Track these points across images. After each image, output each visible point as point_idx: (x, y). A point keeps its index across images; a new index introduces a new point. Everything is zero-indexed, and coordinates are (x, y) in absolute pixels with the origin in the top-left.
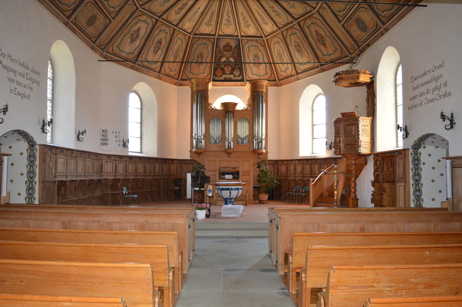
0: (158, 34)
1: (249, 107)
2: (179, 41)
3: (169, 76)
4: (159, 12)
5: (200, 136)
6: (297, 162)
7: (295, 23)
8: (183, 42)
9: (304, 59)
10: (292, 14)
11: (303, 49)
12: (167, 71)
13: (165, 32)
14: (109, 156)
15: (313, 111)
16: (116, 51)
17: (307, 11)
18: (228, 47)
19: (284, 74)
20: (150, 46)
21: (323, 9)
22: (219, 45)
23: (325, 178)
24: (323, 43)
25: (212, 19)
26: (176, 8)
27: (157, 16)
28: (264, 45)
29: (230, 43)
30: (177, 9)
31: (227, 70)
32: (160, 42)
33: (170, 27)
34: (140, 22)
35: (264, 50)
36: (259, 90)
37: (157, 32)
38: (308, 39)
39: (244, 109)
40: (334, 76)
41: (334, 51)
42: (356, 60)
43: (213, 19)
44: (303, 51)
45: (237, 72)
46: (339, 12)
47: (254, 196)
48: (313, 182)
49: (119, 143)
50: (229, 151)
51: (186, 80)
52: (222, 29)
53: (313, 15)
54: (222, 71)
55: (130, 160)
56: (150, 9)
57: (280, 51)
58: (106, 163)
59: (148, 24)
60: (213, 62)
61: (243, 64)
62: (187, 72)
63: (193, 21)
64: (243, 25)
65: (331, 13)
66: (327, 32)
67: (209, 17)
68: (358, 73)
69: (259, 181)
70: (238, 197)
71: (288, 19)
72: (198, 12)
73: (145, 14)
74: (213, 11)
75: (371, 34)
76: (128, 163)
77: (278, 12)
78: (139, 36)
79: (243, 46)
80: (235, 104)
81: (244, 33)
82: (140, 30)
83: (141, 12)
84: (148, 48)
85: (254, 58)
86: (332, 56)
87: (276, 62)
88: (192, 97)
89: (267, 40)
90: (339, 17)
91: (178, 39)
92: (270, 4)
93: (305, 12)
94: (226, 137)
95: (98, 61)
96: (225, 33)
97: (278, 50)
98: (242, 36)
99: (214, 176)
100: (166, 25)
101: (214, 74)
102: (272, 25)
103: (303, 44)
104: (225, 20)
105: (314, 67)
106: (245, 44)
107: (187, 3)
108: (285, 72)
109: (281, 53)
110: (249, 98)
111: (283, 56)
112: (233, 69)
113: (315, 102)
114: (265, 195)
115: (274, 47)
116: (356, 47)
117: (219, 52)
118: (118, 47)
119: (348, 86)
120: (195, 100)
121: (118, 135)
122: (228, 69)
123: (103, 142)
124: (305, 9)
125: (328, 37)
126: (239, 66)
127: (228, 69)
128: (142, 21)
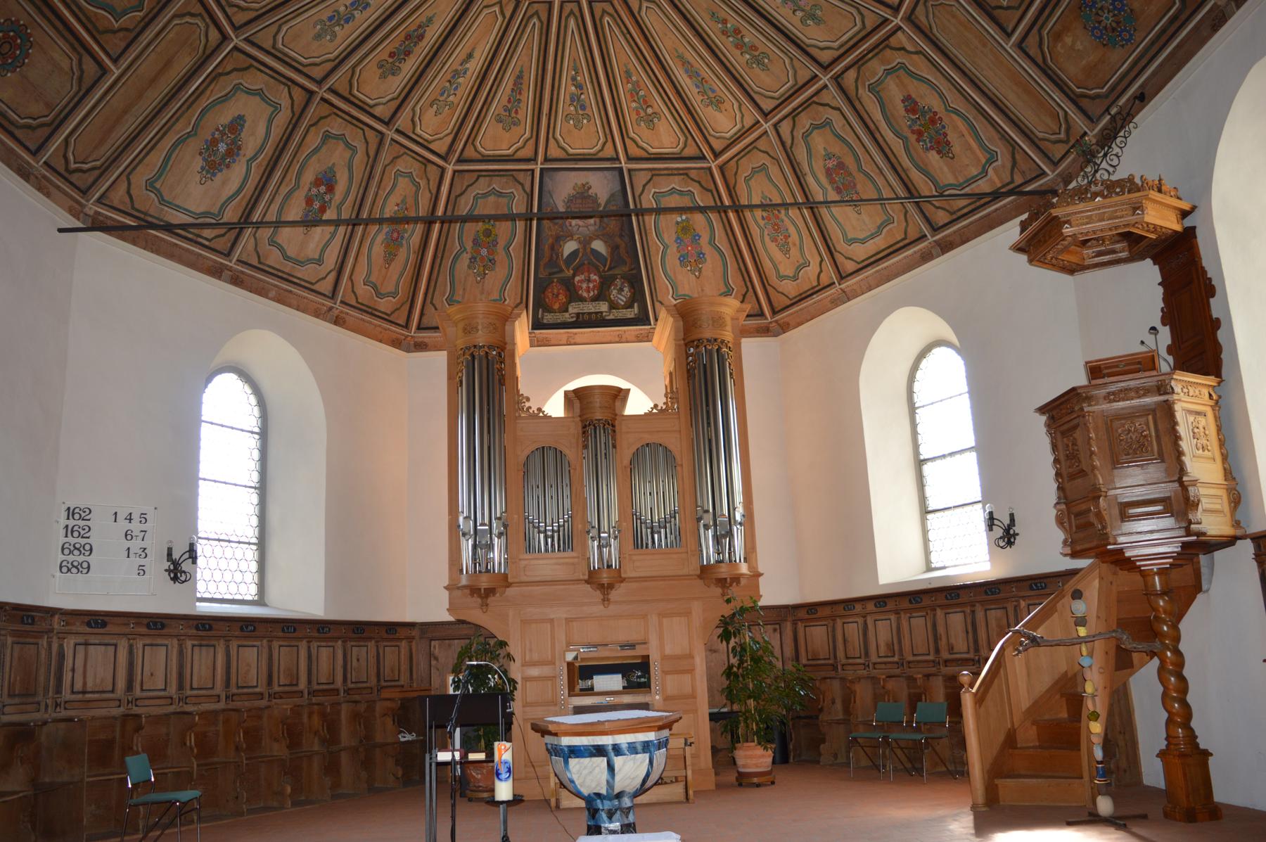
2: (403, 183)
5: (486, 521)
6: (870, 606)
8: (418, 186)
10: (808, 49)
11: (859, 178)
14: (97, 620)
15: (912, 409)
16: (148, 202)
18: (583, 207)
19: (790, 288)
20: (290, 193)
23: (1017, 664)
28: (712, 187)
31: (584, 286)
33: (365, 128)
34: (242, 97)
37: (314, 140)
38: (878, 136)
39: (655, 411)
41: (984, 167)
42: (1105, 155)
43: (523, 97)
45: (621, 290)
47: (715, 750)
48: (972, 686)
49: (142, 562)
50: (605, 578)
53: (891, 39)
54: (569, 290)
55: (201, 633)
58: (81, 649)
59: (276, 107)
63: (453, 107)
64: (634, 116)
66: (951, 96)
69: (730, 694)
70: (649, 783)
72: (465, 73)
76: (189, 643)
77: (756, 49)
78: (239, 148)
79: (637, 194)
80: (619, 395)
82: (243, 126)
85: (678, 238)
89: (721, 169)
91: (399, 174)
92: (725, 22)
94: (591, 523)
95: (61, 230)
96: (571, 151)
99: (550, 683)
101: (540, 304)
102: (736, 106)
103: (858, 160)
104: (568, 101)
106: (644, 186)
107: (421, 31)
108: (795, 278)
114: (760, 751)
115: (749, 187)
118: (150, 185)
120: (461, 385)
121: (135, 526)
122: (589, 281)
123: (71, 558)
125: (956, 112)
126: (626, 269)
127: (589, 281)
128: (250, 92)
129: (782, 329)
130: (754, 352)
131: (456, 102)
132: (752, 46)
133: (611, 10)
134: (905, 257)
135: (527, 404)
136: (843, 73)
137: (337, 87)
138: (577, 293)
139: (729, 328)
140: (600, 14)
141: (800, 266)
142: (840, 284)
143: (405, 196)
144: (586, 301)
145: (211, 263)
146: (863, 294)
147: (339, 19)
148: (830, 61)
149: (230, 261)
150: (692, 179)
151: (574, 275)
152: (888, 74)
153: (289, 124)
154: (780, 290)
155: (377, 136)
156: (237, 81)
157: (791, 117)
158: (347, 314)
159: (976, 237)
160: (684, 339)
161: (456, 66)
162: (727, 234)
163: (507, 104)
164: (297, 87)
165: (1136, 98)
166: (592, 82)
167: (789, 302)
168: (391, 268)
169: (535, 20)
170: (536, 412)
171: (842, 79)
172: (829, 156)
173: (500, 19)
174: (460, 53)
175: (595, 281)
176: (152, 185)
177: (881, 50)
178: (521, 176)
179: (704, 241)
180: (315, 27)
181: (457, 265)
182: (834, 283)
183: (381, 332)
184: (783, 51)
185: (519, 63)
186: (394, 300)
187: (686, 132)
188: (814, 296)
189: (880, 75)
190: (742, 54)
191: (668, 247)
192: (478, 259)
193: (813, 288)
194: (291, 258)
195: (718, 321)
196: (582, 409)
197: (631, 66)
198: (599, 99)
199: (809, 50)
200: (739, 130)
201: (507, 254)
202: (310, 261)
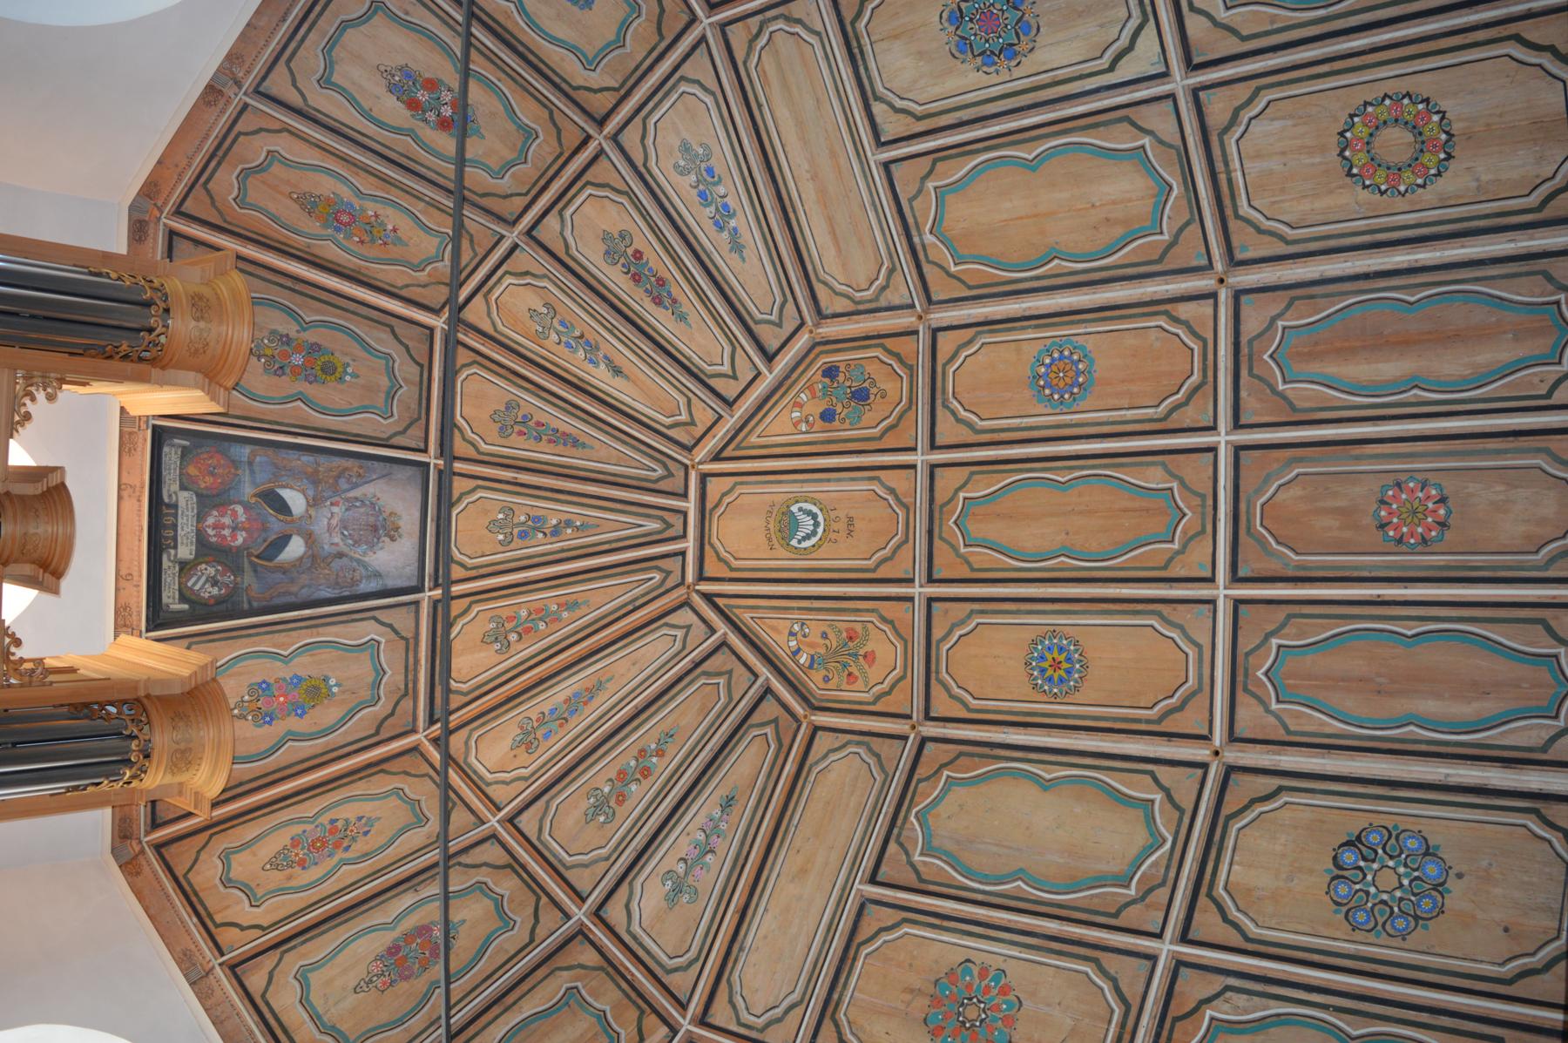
3: (219, 153)
4: (649, 141)
9: (352, 1000)
19: (207, 874)
28: (384, 735)
31: (227, 520)
33: (529, 198)
37: (528, 113)
38: (496, 1010)
39: (7, 640)
43: (544, 446)
45: (215, 583)
52: (480, 494)
53: (653, 1017)
56: (683, 87)
57: (361, 839)
63: (539, 338)
64: (505, 613)
67: (556, 424)
72: (591, 361)
77: (620, 803)
79: (377, 614)
85: (300, 679)
89: (415, 749)
92: (660, 753)
106: (390, 626)
107: (667, 302)
108: (227, 882)
110: (72, 670)
115: (386, 795)
122: (235, 529)
127: (235, 529)
128: (625, 26)
129: (127, 863)
130: (101, 820)
131: (546, 343)
132: (624, 796)
133: (670, 583)
137: (603, 161)
139: (169, 779)
140: (664, 567)
141: (251, 889)
142: (220, 965)
143: (407, 245)
144: (198, 522)
146: (206, 1010)
148: (608, 920)
152: (599, 1017)
153: (561, 77)
154: (203, 856)
155: (511, 214)
156: (644, 11)
157: (511, 861)
158: (223, 111)
160: (148, 696)
161: (605, 349)
162: (302, 761)
163: (535, 419)
164: (614, 102)
166: (563, 550)
167: (180, 872)
168: (289, 202)
169: (660, 472)
170: (23, 410)
171: (581, 943)
173: (668, 421)
174: (625, 357)
175: (234, 537)
177: (634, 1003)
178: (416, 431)
179: (294, 724)
181: (277, 314)
182: (222, 955)
183: (177, 166)
184: (619, 844)
185: (597, 444)
186: (230, 198)
187: (477, 693)
188: (195, 919)
189: (596, 1004)
190: (610, 780)
191: (286, 663)
192: (286, 348)
193: (210, 916)
194: (341, 35)
195: (184, 758)
196: (22, 499)
197: (584, 610)
198: (536, 560)
199: (625, 887)
200: (481, 778)
201: (292, 396)
202: (330, 65)
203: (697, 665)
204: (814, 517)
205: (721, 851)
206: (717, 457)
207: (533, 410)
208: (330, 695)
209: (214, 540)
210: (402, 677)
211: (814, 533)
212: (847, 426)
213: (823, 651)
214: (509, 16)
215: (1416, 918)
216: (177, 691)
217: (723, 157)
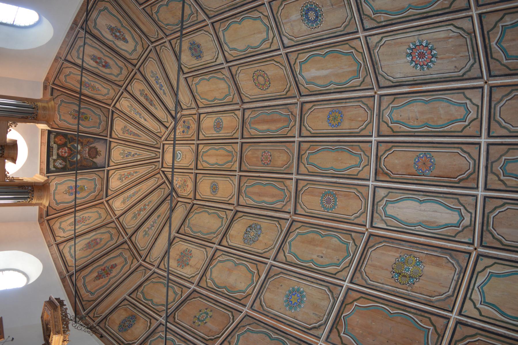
0: (117, 64)
1: (9, 180)
3: (59, 72)
7: (126, 238)
8: (104, 96)
10: (136, 233)
11: (92, 250)
12: (67, 71)
13: (118, 75)
17: (140, 252)
18: (94, 153)
19: (56, 227)
20: (102, 52)
21: (144, 271)
22: (98, 142)
24: (100, 276)
25: (131, 134)
26: (148, 91)
27: (140, 66)
29: (99, 156)
30: (146, 92)
31: (63, 151)
32: (106, 66)
33: (124, 81)
34: (134, 44)
35: (89, 200)
36: (35, 194)
37: (120, 64)
39: (6, 173)
40: (58, 297)
41: (90, 291)
42: (81, 325)
43: (132, 136)
44: (89, 250)
45: (61, 164)
46: (142, 293)
51: (52, 95)
54: (62, 145)
56: (150, 59)
59: (131, 54)
60: (80, 134)
61: (75, 172)
62: (63, 97)
63: (130, 112)
64: (122, 173)
65: (140, 283)
67: (134, 131)
68: (64, 332)
71: (130, 228)
72: (140, 117)
73: (143, 52)
74: (141, 137)
75: (118, 338)
77: (139, 215)
78: (117, 39)
79: (96, 173)
81: (112, 174)
82: (125, 42)
83: (147, 46)
84: (100, 48)
86: (84, 289)
87: (77, 214)
88: (27, 99)
89: (102, 203)
90: (135, 293)
91: (109, 90)
92: (148, 205)
93: (139, 249)
96: (113, 150)
97: (90, 218)
98: (108, 171)
100: (127, 76)
101: (58, 134)
102: (122, 208)
105: (67, 266)
106: (98, 175)
107: (153, 105)
108: (60, 228)
109: (86, 222)
110: (22, 180)
111: (81, 224)
112: (64, 159)
113: (16, 273)
115: (95, 212)
116: (97, 320)
117: (89, 141)
118: (106, 8)
119: (44, 320)
120: (23, 103)
122: (65, 153)
124: (143, 249)
126: (69, 167)
127: (65, 153)
128: (136, 47)
130: (33, 211)
133: (156, 168)
134: (61, 266)
135: (13, 126)
136: (127, 244)
138: (61, 148)
145: (78, 21)
147: (157, 80)
149: (79, 28)
150: (99, 192)
151: (68, 147)
154: (56, 222)
158: (59, 64)
159: (66, 290)
160: (34, 185)
161: (143, 115)
165: (102, 335)
166: (135, 160)
169: (155, 143)
172: (101, 240)
173: (156, 131)
175: (65, 155)
176: (106, 9)
177: (133, 256)
180: (155, 71)
185: (143, 136)
188: (52, 235)
197: (138, 173)
198: (129, 162)
200: (114, 209)
203: (159, 186)
204: (180, 154)
205: (155, 227)
206: (166, 140)
207: (130, 128)
208: (85, 190)
209: (61, 155)
210: (101, 187)
211: (180, 158)
212: (186, 134)
213: (181, 184)
214: (112, 45)
215: (254, 241)
216: (41, 185)
217: (159, 75)
